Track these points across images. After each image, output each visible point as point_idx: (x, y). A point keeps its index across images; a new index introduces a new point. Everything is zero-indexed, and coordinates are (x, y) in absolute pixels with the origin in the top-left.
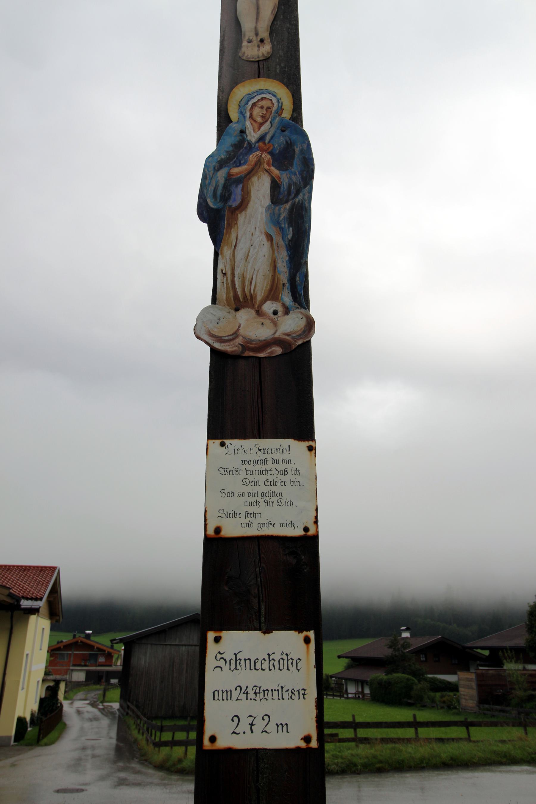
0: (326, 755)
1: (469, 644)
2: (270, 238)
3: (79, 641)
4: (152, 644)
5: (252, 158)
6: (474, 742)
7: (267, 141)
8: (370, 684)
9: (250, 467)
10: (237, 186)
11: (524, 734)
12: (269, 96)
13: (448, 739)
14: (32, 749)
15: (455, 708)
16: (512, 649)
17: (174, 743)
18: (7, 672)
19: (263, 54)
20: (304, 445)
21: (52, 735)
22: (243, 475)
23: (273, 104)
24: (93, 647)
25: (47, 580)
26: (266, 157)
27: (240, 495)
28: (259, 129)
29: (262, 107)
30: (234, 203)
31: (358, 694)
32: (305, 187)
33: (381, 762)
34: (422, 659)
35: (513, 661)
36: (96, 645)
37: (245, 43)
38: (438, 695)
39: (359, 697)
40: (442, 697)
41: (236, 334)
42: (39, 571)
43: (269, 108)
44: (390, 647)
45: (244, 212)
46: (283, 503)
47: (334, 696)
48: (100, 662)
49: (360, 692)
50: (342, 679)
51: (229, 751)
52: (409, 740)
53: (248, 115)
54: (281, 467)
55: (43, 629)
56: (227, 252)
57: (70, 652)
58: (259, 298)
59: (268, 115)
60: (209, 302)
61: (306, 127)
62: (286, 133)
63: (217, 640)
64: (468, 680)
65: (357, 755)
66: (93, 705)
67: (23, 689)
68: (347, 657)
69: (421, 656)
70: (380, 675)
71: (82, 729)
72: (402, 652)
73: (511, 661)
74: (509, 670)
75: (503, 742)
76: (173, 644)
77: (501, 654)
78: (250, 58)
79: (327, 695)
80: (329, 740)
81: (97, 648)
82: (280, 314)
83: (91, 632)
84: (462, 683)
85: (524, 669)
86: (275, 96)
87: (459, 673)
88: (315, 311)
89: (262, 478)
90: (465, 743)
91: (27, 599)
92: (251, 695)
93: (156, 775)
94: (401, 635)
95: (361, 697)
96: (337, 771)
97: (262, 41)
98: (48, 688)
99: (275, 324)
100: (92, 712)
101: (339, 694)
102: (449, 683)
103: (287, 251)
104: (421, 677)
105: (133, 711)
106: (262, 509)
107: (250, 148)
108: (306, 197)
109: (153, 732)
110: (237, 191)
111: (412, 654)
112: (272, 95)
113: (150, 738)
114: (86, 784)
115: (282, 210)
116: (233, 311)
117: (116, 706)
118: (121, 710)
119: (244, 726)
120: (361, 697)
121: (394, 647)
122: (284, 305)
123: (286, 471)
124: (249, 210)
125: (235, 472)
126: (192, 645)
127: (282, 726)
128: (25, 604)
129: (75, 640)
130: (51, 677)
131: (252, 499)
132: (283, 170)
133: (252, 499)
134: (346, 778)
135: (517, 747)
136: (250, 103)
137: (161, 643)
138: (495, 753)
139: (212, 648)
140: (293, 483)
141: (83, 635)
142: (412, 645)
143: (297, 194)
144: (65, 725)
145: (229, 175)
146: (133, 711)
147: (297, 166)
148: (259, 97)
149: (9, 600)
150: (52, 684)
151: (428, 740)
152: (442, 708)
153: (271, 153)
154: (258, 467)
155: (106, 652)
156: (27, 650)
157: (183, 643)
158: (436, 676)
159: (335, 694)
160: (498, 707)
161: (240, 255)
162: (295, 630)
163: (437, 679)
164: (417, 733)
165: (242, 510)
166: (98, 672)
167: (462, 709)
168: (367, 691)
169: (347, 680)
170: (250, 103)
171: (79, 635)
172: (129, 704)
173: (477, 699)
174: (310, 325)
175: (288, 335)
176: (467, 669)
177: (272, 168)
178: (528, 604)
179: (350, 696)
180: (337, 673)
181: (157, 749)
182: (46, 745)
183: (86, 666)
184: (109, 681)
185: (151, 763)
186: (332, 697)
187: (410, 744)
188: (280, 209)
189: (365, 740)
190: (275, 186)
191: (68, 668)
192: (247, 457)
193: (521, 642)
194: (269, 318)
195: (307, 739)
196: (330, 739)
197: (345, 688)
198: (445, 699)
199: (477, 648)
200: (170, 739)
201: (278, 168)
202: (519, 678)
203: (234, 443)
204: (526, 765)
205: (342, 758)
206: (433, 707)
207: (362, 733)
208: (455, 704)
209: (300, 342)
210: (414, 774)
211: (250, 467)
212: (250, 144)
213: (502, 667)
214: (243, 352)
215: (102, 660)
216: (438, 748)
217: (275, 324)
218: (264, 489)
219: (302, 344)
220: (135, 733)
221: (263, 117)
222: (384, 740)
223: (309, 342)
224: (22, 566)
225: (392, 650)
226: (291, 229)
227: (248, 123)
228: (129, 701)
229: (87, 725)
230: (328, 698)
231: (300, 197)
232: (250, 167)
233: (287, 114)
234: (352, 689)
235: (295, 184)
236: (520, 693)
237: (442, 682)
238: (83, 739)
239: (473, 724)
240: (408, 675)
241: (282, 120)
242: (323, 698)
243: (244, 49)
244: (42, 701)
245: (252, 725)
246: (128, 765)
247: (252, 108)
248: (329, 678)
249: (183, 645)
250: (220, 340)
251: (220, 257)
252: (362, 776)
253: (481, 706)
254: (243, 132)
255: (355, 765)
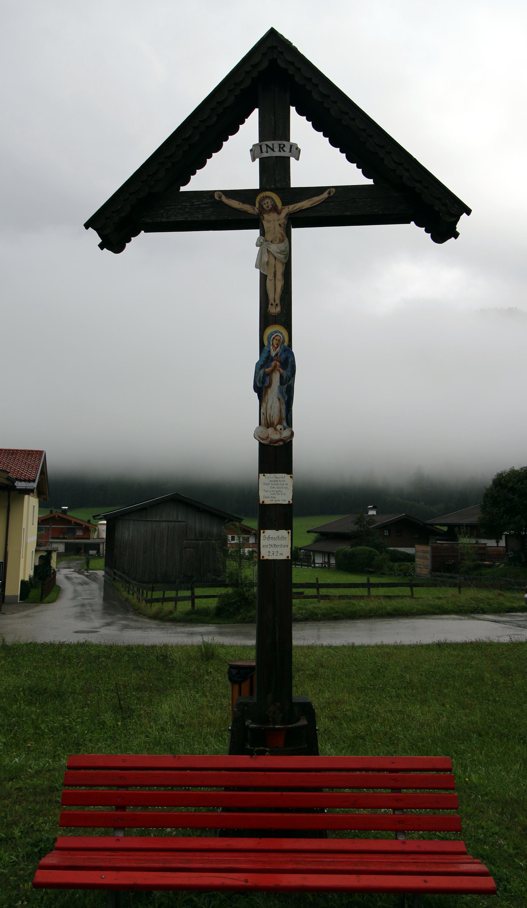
0: (293, 608)
1: (430, 521)
2: (279, 399)
3: (57, 516)
4: (134, 520)
5: (273, 364)
6: (415, 598)
7: (278, 356)
8: (336, 555)
9: (273, 483)
10: (267, 377)
11: (457, 592)
12: (279, 334)
13: (395, 596)
14: (38, 606)
15: (411, 575)
16: (467, 526)
17: (164, 600)
18: (8, 543)
19: (277, 312)
20: (289, 476)
21: (52, 595)
22: (270, 485)
23: (281, 338)
24: (71, 521)
25: (10, 458)
26: (278, 364)
27: (270, 491)
28: (276, 350)
29: (277, 340)
30: (266, 384)
31: (324, 564)
32: (292, 378)
33: (337, 612)
34: (385, 534)
35: (467, 536)
36: (73, 520)
37: (270, 306)
38: (396, 564)
39: (325, 566)
40: (399, 566)
41: (268, 437)
42: (27, 455)
43: (279, 340)
44: (356, 523)
45: (270, 389)
46: (282, 494)
47: (302, 565)
48: (77, 535)
49: (326, 562)
50: (310, 551)
51: (267, 560)
52: (362, 597)
53: (271, 343)
54: (282, 483)
55: (34, 506)
56: (264, 405)
57: (49, 526)
58: (275, 424)
59: (279, 343)
60: (258, 425)
61: (294, 350)
62: (286, 352)
63: (264, 532)
64: (424, 552)
65: (319, 608)
66: (80, 572)
67: (23, 557)
68: (315, 532)
69: (385, 531)
70: (346, 548)
71: (75, 591)
72: (367, 528)
73: (465, 536)
74: (461, 544)
75: (439, 598)
76: (154, 520)
77: (456, 529)
78: (272, 314)
79: (296, 565)
80: (296, 597)
81: (75, 522)
82: (282, 430)
83: (67, 508)
84: (419, 554)
85: (477, 543)
86: (282, 335)
87: (416, 546)
88: (294, 429)
89: (276, 486)
90: (408, 599)
91: (21, 481)
92: (273, 546)
93: (153, 623)
94: (368, 513)
95: (327, 566)
96: (302, 619)
97: (277, 305)
98: (41, 557)
99: (281, 433)
100: (80, 578)
101: (307, 564)
102: (409, 555)
103: (285, 405)
104: (383, 549)
105: (120, 577)
106: (276, 496)
107: (272, 360)
108: (292, 382)
109: (145, 591)
110: (268, 379)
111: (376, 529)
112: (281, 334)
113: (142, 597)
114: (97, 628)
115: (284, 388)
116: (266, 428)
117: (101, 573)
118: (107, 576)
119: (271, 554)
120: (327, 566)
121: (360, 524)
122: (284, 426)
123: (283, 484)
124: (272, 388)
125: (268, 484)
126: (172, 521)
127: (281, 554)
128: (19, 485)
129: (52, 515)
130: (43, 548)
131: (273, 493)
132: (284, 370)
133: (273, 493)
134: (309, 623)
135: (450, 602)
136: (272, 337)
137: (143, 520)
138: (431, 606)
139: (262, 535)
140: (286, 488)
141: (59, 511)
142: (376, 521)
143: (290, 380)
144: (59, 587)
145: (265, 372)
146: (120, 577)
147: (289, 369)
148: (276, 334)
149: (6, 482)
150: (44, 554)
151: (377, 597)
152: (399, 575)
153: (280, 362)
154: (275, 483)
155: (84, 526)
156: (24, 526)
157: (163, 519)
158: (397, 549)
159: (303, 564)
160: (448, 574)
161: (269, 407)
162: (285, 530)
163: (397, 550)
164: (369, 591)
165: (270, 496)
166: (77, 544)
167: (416, 576)
168: (333, 561)
169: (315, 552)
170: (272, 337)
171: (56, 510)
172: (115, 571)
173: (430, 568)
174: (292, 434)
175: (285, 438)
176: (427, 544)
177: (280, 369)
178: (485, 487)
179: (317, 565)
180: (305, 546)
181: (149, 605)
182: (49, 602)
183: (64, 538)
184: (89, 552)
185: (145, 615)
186: (300, 567)
187: (363, 600)
188: (283, 387)
189: (326, 597)
190: (281, 377)
191: (48, 540)
192: (271, 480)
193: (474, 519)
194: (279, 431)
195: (288, 557)
196: (297, 596)
197: (312, 559)
198: (402, 568)
199: (436, 525)
200: (162, 596)
201: (282, 369)
202: (469, 551)
203: (267, 475)
204: (454, 615)
205: (306, 609)
206: (391, 574)
207: (323, 591)
208: (410, 572)
209: (289, 440)
210: (363, 621)
211: (273, 483)
212: (272, 357)
213: (457, 541)
214: (270, 444)
215: (79, 533)
216: (384, 603)
217: (281, 433)
218: (277, 490)
219: (290, 441)
220: (125, 594)
221: (277, 344)
222: (341, 597)
223: (292, 440)
224: (9, 450)
225: (358, 526)
226: (287, 396)
227: (271, 347)
228: (115, 569)
229: (79, 588)
230: (297, 567)
231: (290, 382)
232: (272, 368)
233: (286, 344)
234: (319, 560)
235: (289, 376)
236: (469, 563)
237: (403, 553)
238: (79, 598)
239: (417, 585)
240: (371, 547)
241: (284, 346)
242: (291, 567)
243: (269, 309)
244: (36, 568)
245: (273, 554)
246: (126, 616)
247: (273, 340)
248: (298, 550)
249: (163, 521)
250: (263, 439)
251: (262, 407)
252: (321, 622)
253: (433, 573)
254: (269, 351)
255: (316, 614)
